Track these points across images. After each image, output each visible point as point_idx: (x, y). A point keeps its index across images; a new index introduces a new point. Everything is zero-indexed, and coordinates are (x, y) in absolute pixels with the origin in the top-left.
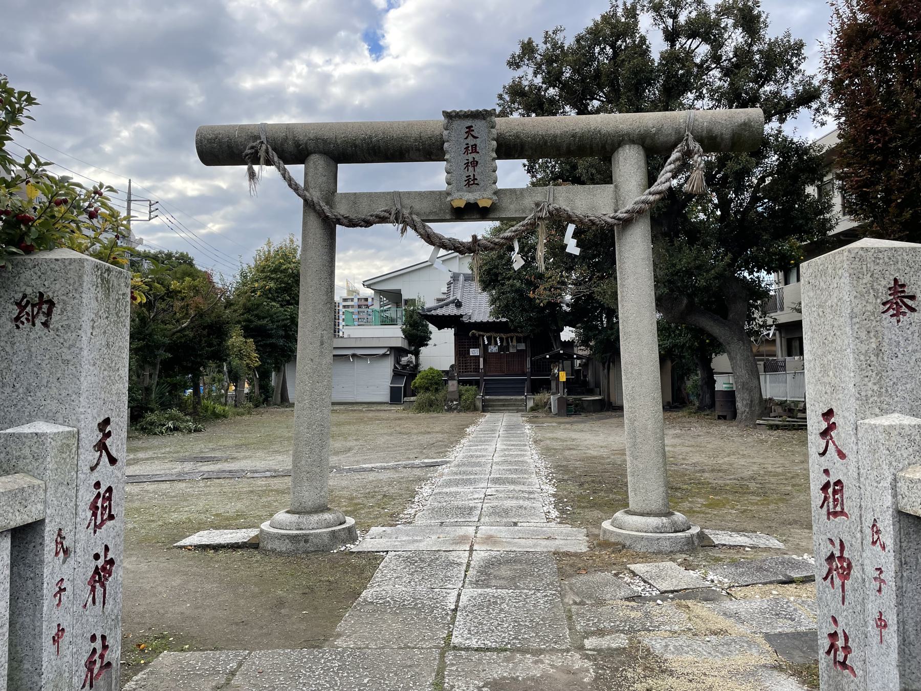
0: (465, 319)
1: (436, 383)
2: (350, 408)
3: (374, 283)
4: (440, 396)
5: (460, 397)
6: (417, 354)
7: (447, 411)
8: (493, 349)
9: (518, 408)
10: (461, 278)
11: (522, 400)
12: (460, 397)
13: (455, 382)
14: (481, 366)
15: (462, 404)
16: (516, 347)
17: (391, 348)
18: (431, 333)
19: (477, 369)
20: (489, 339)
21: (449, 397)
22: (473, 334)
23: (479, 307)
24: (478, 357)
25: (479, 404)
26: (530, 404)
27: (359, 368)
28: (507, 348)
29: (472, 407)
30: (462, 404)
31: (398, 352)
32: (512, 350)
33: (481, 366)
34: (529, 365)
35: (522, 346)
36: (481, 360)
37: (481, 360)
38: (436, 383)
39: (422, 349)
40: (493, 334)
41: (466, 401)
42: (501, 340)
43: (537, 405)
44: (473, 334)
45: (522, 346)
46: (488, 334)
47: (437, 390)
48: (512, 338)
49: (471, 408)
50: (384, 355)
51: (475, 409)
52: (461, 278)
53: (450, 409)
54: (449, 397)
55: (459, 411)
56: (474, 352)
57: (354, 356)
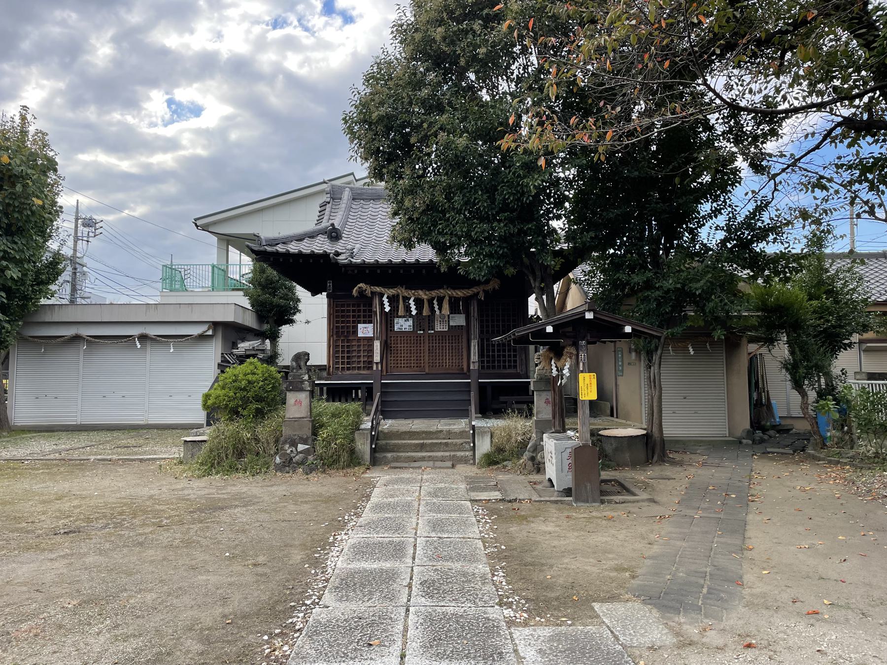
0: (342, 259)
1: (259, 399)
2: (108, 436)
3: (214, 223)
4: (264, 430)
5: (315, 433)
6: (274, 337)
7: (280, 468)
8: (403, 325)
9: (453, 452)
10: (346, 195)
11: (462, 434)
12: (315, 433)
13: (303, 397)
14: (377, 358)
15: (320, 450)
16: (447, 320)
17: (215, 325)
18: (299, 300)
19: (369, 364)
20: (393, 300)
21: (286, 431)
22: (361, 292)
23: (374, 237)
24: (370, 340)
25: (364, 446)
26: (484, 446)
27: (155, 360)
28: (431, 318)
29: (345, 457)
30: (320, 450)
31: (231, 332)
32: (439, 327)
33: (377, 358)
34: (474, 357)
35: (459, 320)
36: (377, 345)
37: (377, 345)
38: (259, 399)
39: (285, 329)
40: (402, 291)
41: (328, 442)
42: (419, 303)
43: (500, 450)
44: (361, 292)
45: (459, 320)
46: (392, 292)
47: (260, 414)
48: (440, 301)
49: (344, 458)
50: (202, 337)
51: (353, 460)
52: (346, 195)
53: (288, 464)
54: (286, 431)
55: (311, 470)
56: (365, 330)
57: (143, 338)
